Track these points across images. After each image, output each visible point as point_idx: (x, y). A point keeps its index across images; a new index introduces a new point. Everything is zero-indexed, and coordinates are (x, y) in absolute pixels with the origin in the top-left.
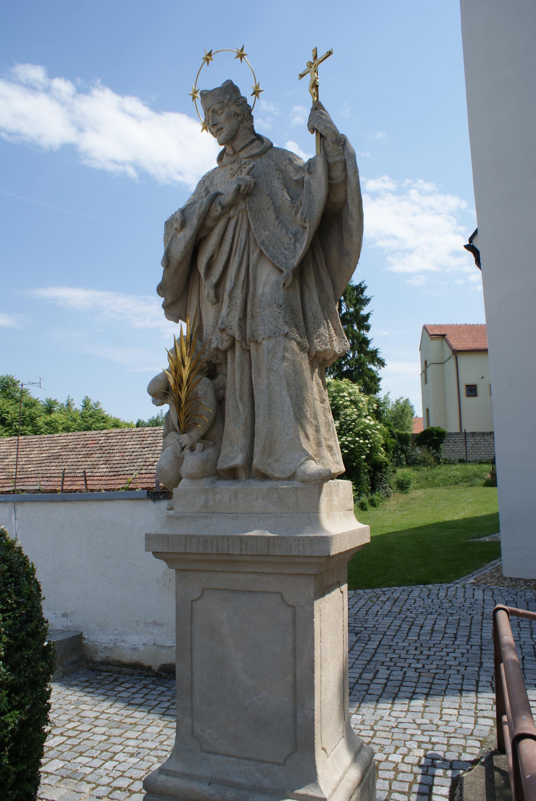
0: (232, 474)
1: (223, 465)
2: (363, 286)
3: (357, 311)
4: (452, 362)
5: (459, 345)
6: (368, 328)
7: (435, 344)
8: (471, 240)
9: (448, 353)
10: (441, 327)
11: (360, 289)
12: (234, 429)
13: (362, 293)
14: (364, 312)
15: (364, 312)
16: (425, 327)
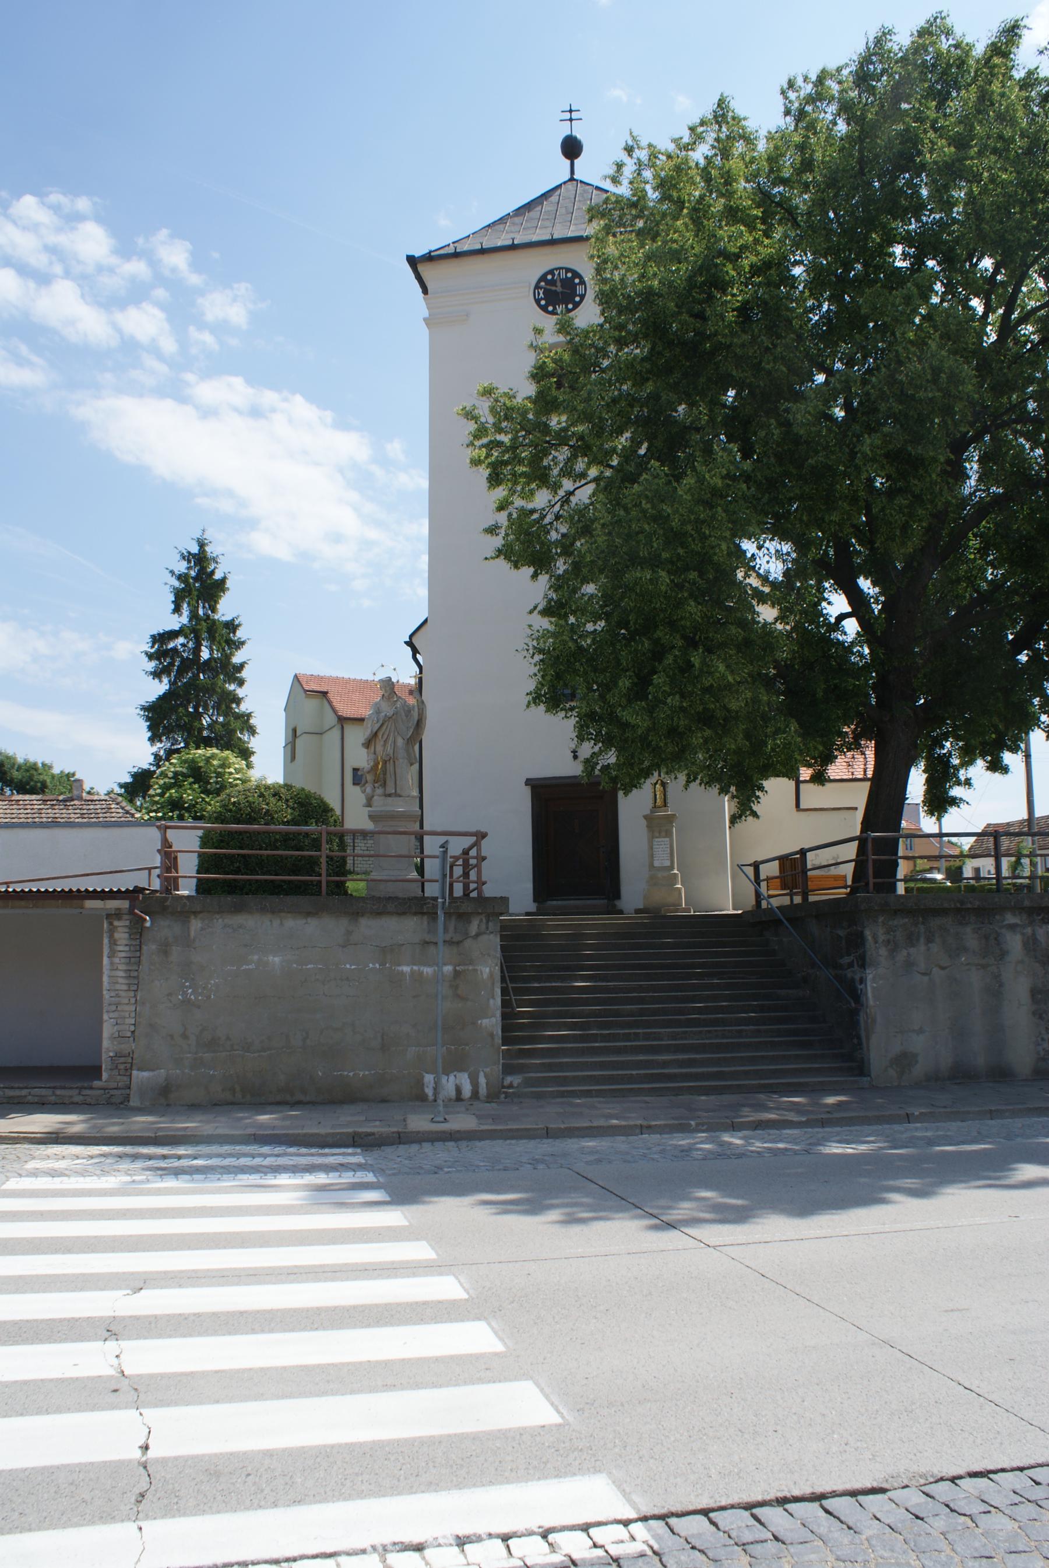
0: (390, 795)
1: (387, 792)
2: (237, 622)
3: (228, 657)
4: (336, 733)
5: (346, 711)
6: (241, 683)
7: (311, 705)
8: (411, 637)
9: (331, 719)
10: (320, 679)
11: (232, 626)
12: (390, 784)
13: (234, 633)
14: (237, 659)
15: (237, 659)
16: (296, 676)
